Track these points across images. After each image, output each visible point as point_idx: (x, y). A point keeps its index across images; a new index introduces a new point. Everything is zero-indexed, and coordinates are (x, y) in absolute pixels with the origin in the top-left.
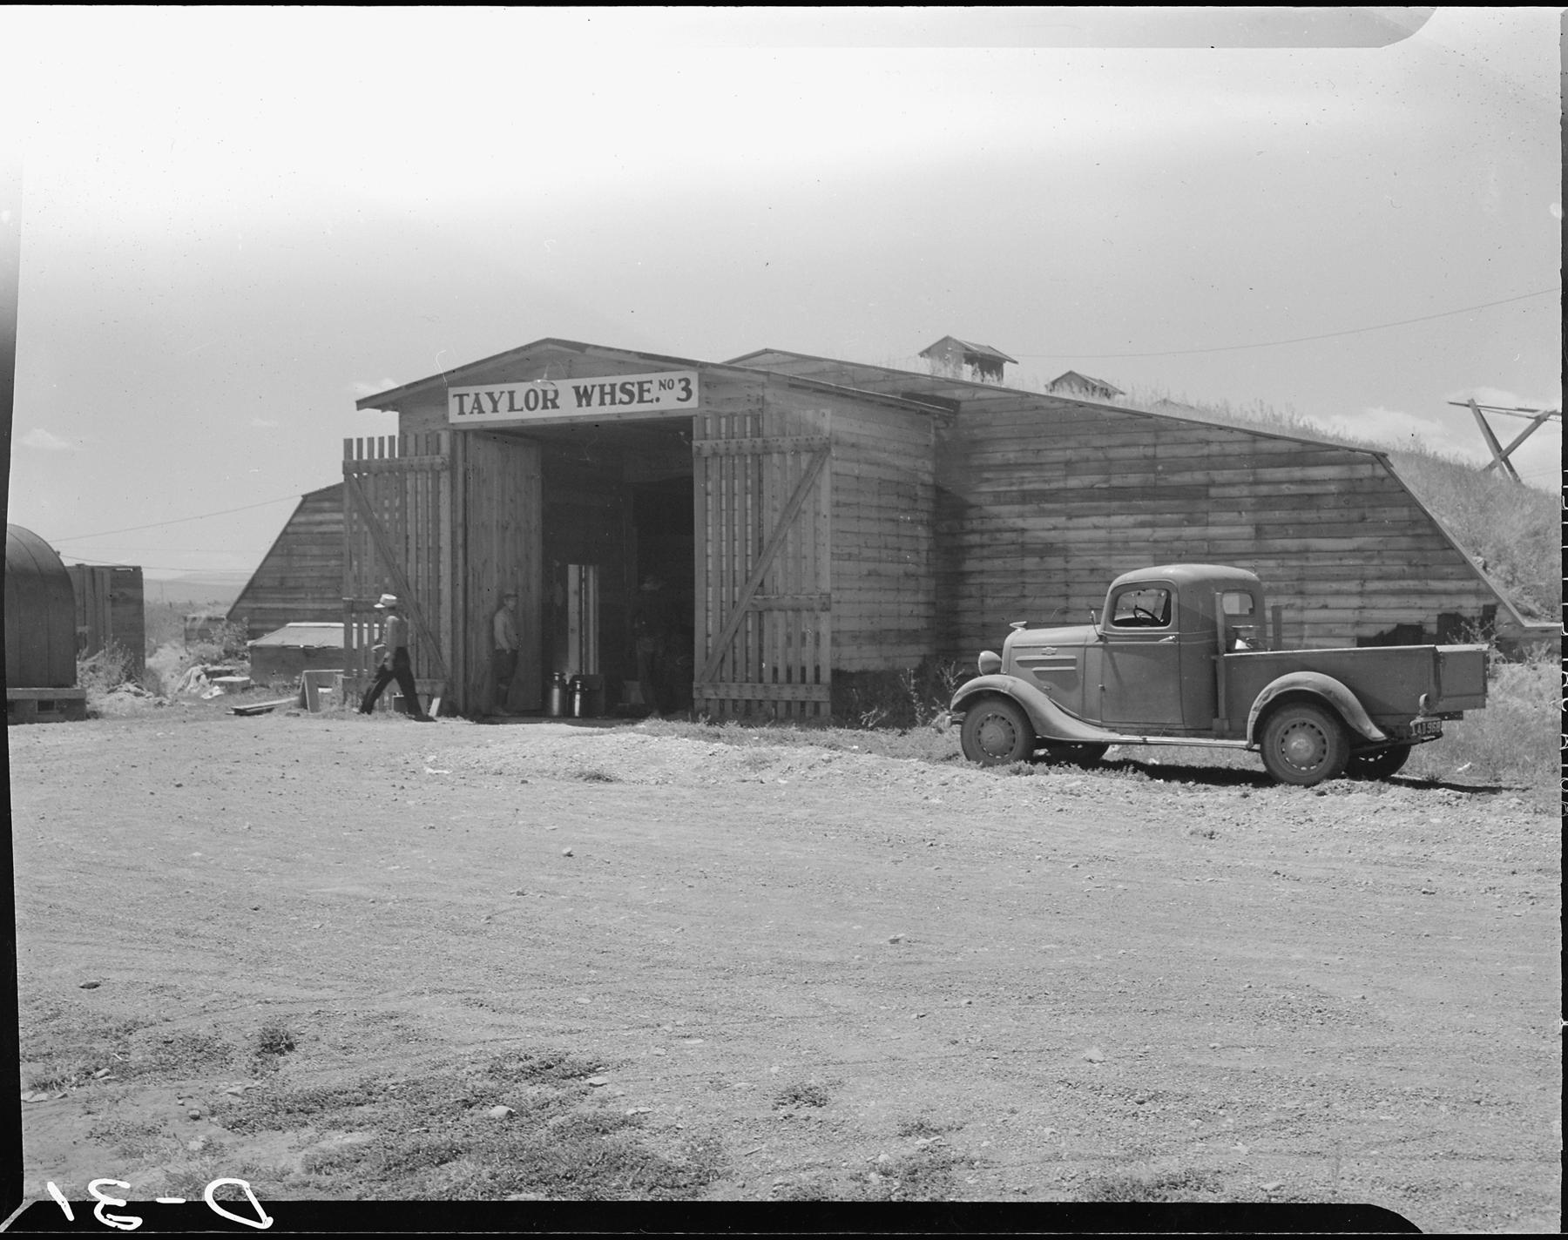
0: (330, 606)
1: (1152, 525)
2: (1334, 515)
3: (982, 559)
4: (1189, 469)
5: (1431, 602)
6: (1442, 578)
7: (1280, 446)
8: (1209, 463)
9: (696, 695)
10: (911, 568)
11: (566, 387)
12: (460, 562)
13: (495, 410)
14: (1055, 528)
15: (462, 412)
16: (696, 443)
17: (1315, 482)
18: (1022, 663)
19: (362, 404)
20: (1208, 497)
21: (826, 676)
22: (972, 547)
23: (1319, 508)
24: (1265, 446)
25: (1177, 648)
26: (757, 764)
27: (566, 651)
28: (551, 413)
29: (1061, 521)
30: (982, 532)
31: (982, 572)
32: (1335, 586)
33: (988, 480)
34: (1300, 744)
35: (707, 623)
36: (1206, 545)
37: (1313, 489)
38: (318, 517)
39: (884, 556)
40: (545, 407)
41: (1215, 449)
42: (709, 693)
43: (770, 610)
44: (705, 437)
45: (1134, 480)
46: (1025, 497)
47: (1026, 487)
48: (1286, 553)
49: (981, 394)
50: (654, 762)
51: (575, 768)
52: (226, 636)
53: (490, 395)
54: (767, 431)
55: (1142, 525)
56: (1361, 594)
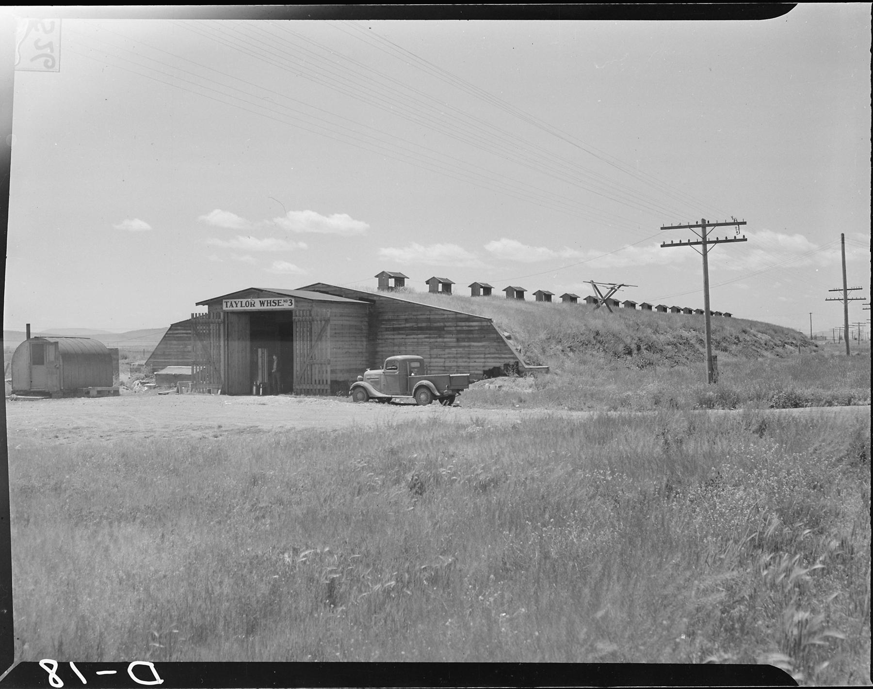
0: (180, 361)
1: (429, 338)
2: (477, 336)
3: (382, 347)
4: (439, 322)
5: (502, 360)
6: (505, 354)
7: (463, 316)
8: (444, 320)
9: (294, 388)
10: (360, 350)
11: (257, 301)
12: (226, 350)
13: (237, 306)
14: (403, 338)
15: (227, 307)
16: (293, 318)
17: (472, 326)
18: (368, 379)
19: (197, 304)
20: (444, 330)
21: (329, 382)
22: (379, 344)
23: (473, 334)
24: (459, 316)
25: (399, 375)
26: (300, 402)
27: (258, 376)
28: (253, 308)
29: (404, 336)
30: (382, 339)
31: (382, 351)
32: (478, 356)
33: (384, 324)
34: (423, 397)
35: (297, 367)
36: (444, 344)
37: (472, 328)
38: (177, 332)
39: (351, 347)
40: (251, 306)
41: (446, 316)
42: (298, 387)
43: (314, 364)
44: (296, 316)
45: (424, 325)
46: (394, 329)
47: (395, 326)
48: (464, 347)
49: (381, 299)
50: (277, 401)
51: (259, 403)
52: (145, 370)
53: (235, 302)
54: (313, 315)
55: (426, 338)
56: (485, 358)
